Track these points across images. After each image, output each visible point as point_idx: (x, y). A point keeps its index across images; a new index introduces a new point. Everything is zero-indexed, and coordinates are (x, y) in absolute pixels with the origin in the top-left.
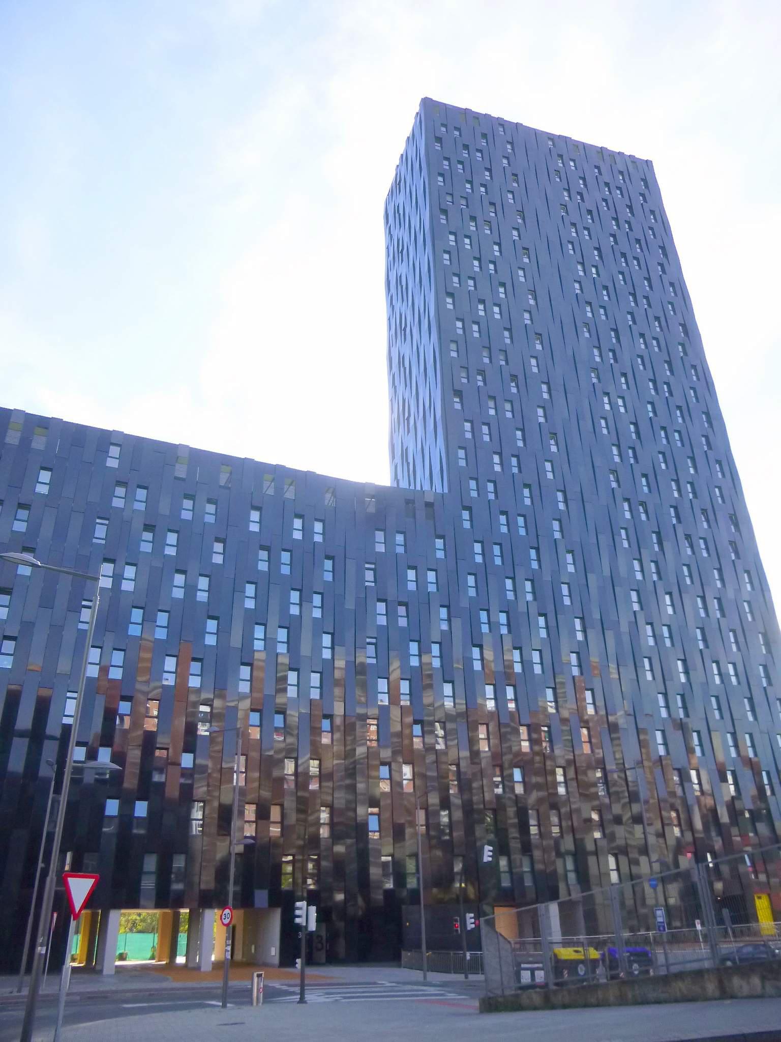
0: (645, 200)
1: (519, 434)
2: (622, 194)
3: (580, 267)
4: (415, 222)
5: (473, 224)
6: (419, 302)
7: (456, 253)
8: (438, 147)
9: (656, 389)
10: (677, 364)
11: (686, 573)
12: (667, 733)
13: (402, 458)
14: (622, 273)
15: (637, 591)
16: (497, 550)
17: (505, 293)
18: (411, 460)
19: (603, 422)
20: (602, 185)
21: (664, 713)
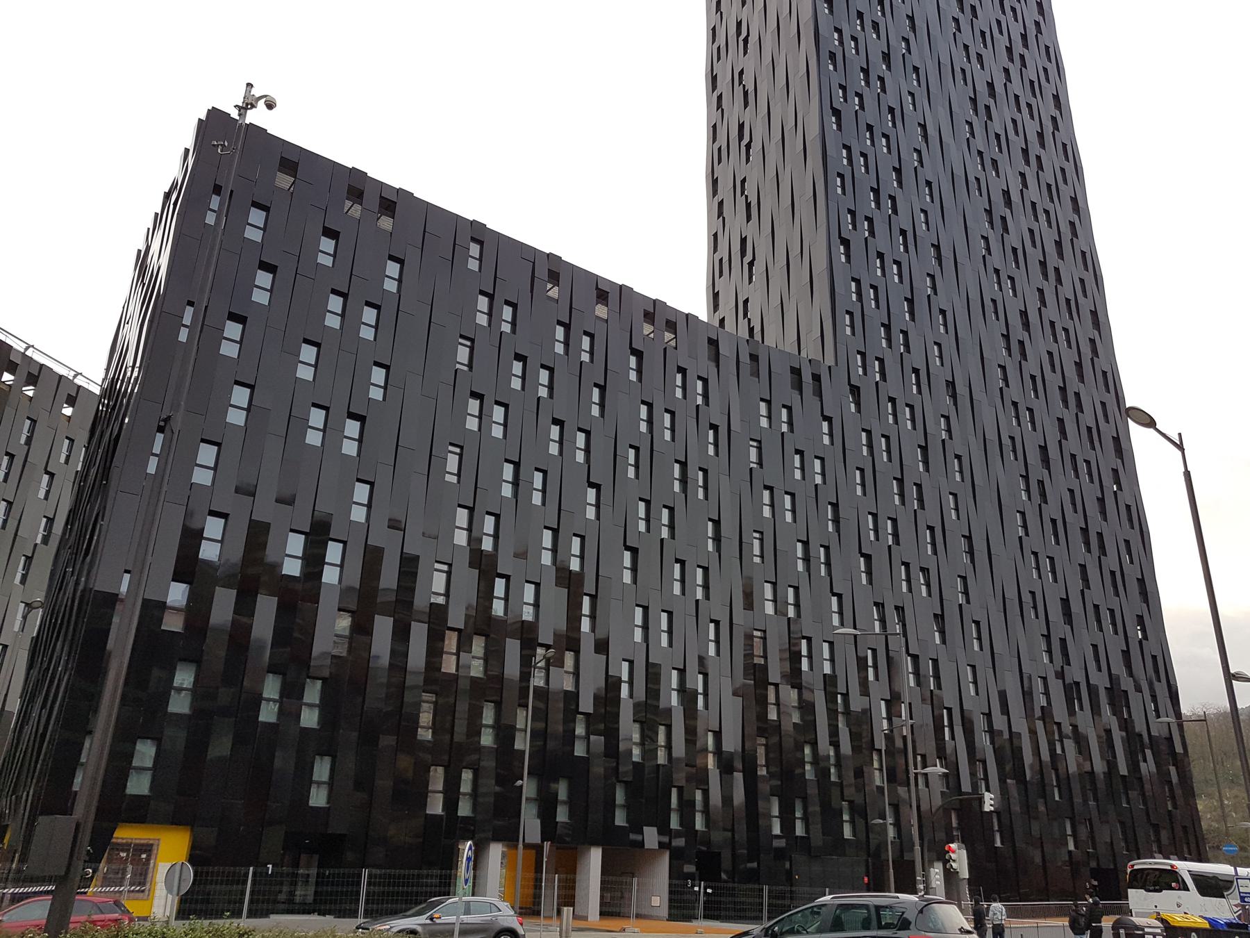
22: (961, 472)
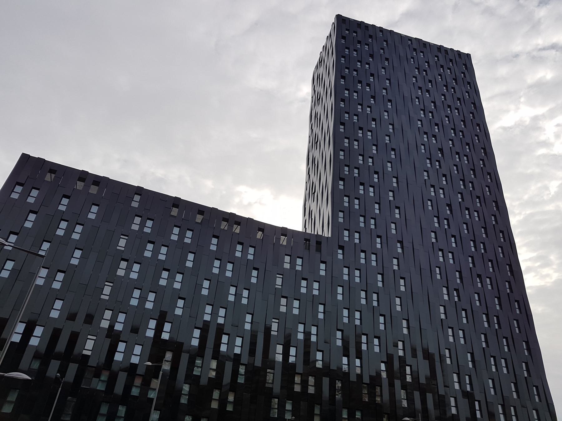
0: (465, 76)
1: (380, 277)
2: (459, 113)
3: (428, 161)
4: (327, 83)
5: (360, 85)
6: (325, 127)
7: (349, 213)
8: (343, 41)
9: (464, 185)
10: (478, 171)
11: (477, 298)
12: (458, 400)
13: (308, 213)
14: (456, 166)
15: (444, 307)
16: (357, 273)
17: (378, 178)
18: (313, 218)
19: (429, 203)
20: (485, 173)
21: (457, 386)
22: (538, 395)
